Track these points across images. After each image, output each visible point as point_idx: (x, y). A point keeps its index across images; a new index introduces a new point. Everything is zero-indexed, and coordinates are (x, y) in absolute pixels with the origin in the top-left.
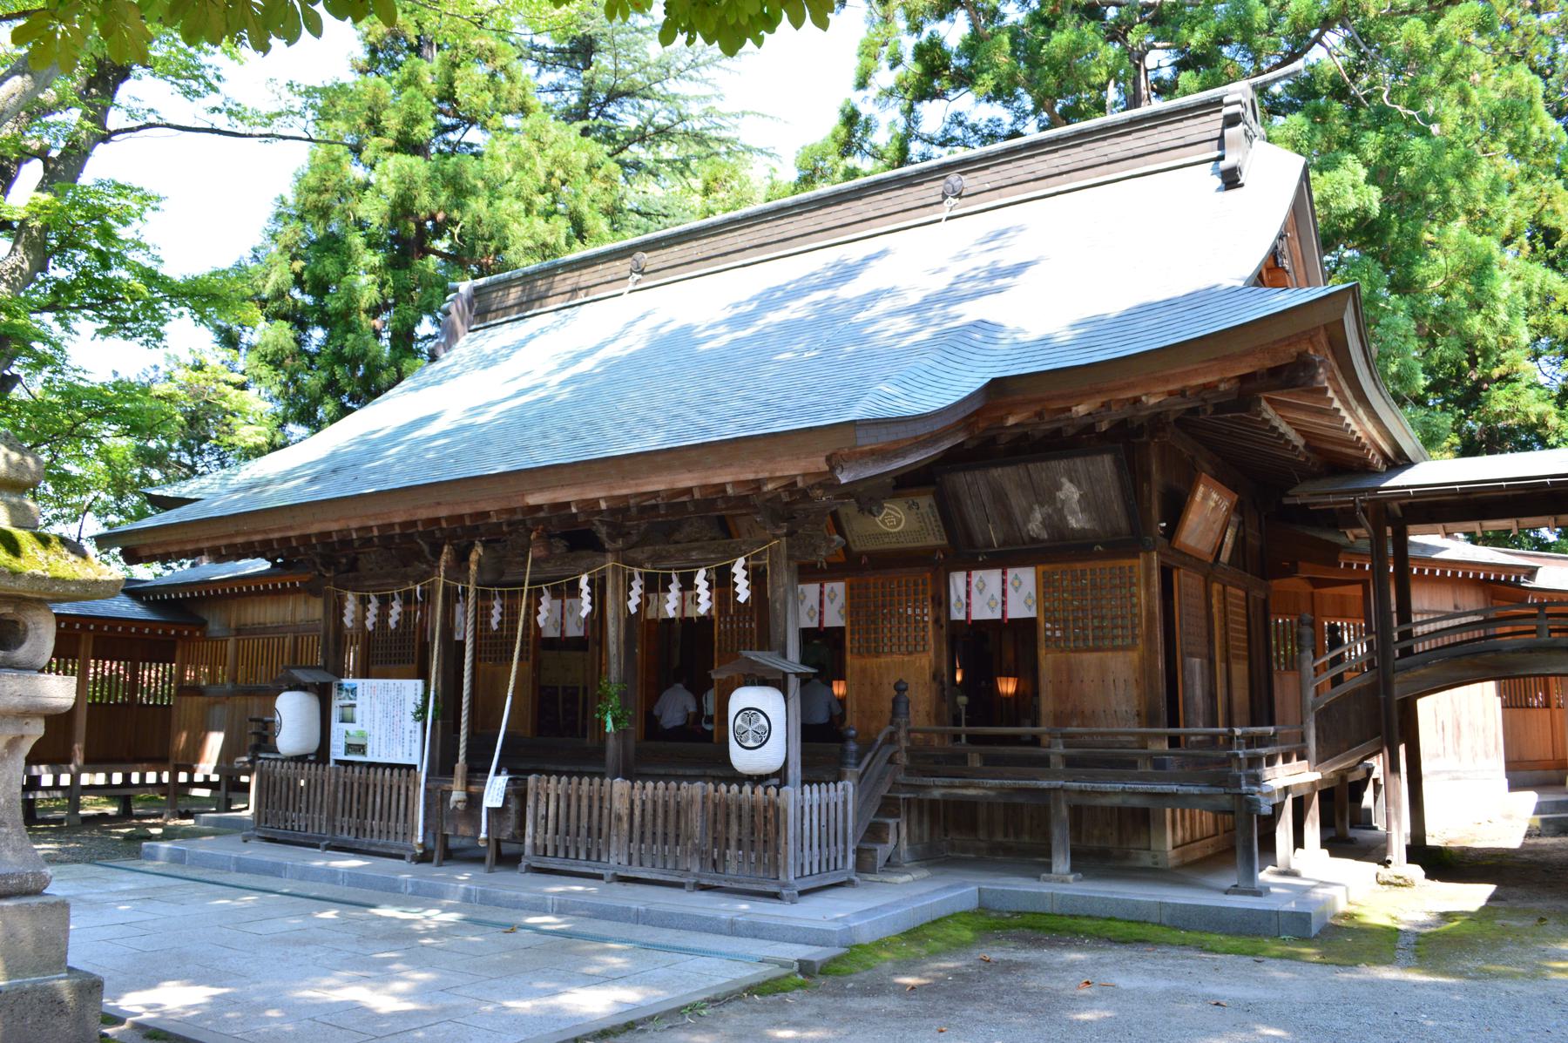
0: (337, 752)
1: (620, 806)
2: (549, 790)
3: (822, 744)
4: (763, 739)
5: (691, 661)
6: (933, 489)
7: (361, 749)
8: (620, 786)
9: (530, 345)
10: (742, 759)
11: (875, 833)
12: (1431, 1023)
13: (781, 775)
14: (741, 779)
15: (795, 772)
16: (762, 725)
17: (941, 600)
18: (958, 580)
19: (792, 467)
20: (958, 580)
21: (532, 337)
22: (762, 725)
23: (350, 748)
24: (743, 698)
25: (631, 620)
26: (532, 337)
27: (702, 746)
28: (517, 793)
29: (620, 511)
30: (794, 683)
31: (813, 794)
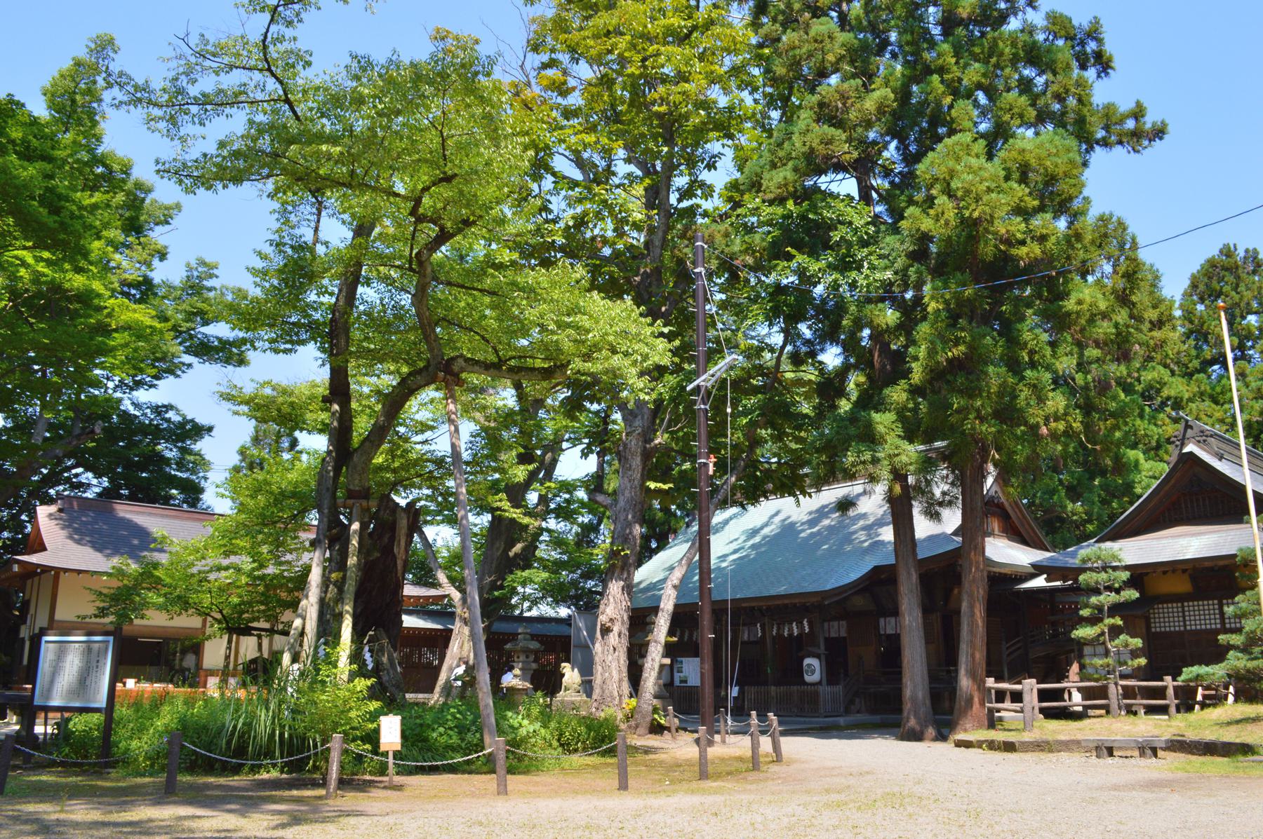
0: (677, 683)
1: (773, 694)
2: (752, 691)
3: (832, 674)
4: (813, 672)
5: (794, 650)
6: (922, 554)
7: (686, 682)
8: (773, 688)
9: (731, 522)
10: (808, 678)
11: (852, 702)
12: (55, 379)
13: (820, 683)
14: (808, 684)
15: (824, 682)
16: (813, 669)
17: (877, 627)
18: (882, 621)
19: (814, 600)
20: (882, 621)
21: (731, 518)
22: (813, 669)
23: (681, 682)
24: (807, 661)
25: (774, 638)
26: (731, 518)
27: (797, 672)
28: (741, 692)
29: (769, 608)
30: (823, 657)
31: (829, 689)
